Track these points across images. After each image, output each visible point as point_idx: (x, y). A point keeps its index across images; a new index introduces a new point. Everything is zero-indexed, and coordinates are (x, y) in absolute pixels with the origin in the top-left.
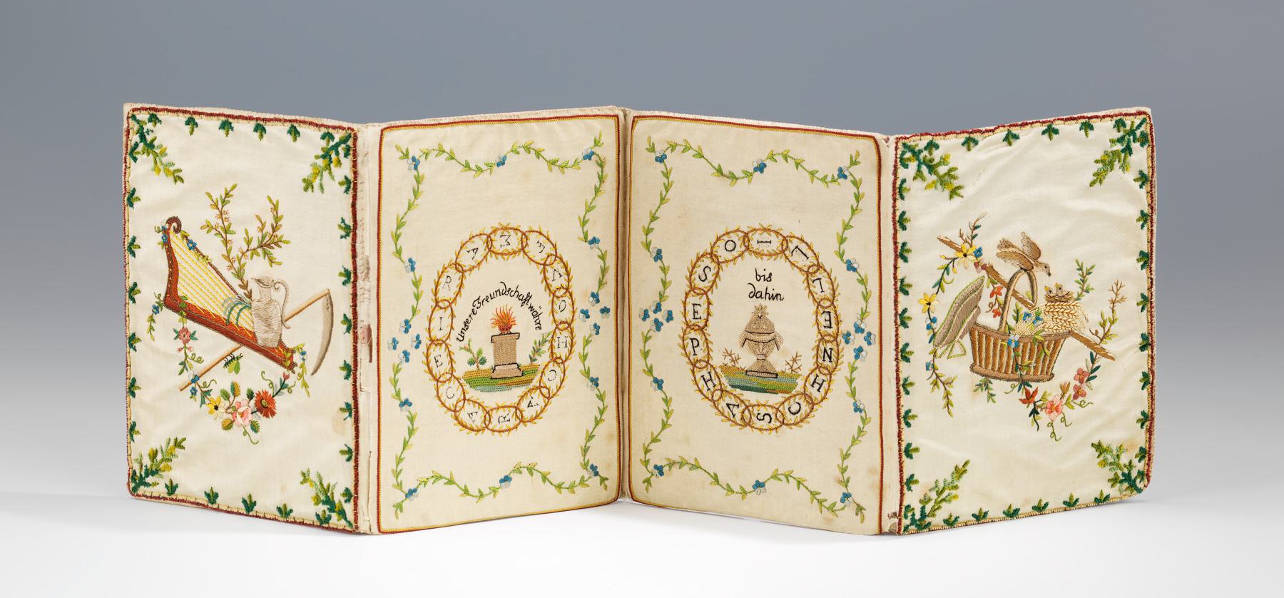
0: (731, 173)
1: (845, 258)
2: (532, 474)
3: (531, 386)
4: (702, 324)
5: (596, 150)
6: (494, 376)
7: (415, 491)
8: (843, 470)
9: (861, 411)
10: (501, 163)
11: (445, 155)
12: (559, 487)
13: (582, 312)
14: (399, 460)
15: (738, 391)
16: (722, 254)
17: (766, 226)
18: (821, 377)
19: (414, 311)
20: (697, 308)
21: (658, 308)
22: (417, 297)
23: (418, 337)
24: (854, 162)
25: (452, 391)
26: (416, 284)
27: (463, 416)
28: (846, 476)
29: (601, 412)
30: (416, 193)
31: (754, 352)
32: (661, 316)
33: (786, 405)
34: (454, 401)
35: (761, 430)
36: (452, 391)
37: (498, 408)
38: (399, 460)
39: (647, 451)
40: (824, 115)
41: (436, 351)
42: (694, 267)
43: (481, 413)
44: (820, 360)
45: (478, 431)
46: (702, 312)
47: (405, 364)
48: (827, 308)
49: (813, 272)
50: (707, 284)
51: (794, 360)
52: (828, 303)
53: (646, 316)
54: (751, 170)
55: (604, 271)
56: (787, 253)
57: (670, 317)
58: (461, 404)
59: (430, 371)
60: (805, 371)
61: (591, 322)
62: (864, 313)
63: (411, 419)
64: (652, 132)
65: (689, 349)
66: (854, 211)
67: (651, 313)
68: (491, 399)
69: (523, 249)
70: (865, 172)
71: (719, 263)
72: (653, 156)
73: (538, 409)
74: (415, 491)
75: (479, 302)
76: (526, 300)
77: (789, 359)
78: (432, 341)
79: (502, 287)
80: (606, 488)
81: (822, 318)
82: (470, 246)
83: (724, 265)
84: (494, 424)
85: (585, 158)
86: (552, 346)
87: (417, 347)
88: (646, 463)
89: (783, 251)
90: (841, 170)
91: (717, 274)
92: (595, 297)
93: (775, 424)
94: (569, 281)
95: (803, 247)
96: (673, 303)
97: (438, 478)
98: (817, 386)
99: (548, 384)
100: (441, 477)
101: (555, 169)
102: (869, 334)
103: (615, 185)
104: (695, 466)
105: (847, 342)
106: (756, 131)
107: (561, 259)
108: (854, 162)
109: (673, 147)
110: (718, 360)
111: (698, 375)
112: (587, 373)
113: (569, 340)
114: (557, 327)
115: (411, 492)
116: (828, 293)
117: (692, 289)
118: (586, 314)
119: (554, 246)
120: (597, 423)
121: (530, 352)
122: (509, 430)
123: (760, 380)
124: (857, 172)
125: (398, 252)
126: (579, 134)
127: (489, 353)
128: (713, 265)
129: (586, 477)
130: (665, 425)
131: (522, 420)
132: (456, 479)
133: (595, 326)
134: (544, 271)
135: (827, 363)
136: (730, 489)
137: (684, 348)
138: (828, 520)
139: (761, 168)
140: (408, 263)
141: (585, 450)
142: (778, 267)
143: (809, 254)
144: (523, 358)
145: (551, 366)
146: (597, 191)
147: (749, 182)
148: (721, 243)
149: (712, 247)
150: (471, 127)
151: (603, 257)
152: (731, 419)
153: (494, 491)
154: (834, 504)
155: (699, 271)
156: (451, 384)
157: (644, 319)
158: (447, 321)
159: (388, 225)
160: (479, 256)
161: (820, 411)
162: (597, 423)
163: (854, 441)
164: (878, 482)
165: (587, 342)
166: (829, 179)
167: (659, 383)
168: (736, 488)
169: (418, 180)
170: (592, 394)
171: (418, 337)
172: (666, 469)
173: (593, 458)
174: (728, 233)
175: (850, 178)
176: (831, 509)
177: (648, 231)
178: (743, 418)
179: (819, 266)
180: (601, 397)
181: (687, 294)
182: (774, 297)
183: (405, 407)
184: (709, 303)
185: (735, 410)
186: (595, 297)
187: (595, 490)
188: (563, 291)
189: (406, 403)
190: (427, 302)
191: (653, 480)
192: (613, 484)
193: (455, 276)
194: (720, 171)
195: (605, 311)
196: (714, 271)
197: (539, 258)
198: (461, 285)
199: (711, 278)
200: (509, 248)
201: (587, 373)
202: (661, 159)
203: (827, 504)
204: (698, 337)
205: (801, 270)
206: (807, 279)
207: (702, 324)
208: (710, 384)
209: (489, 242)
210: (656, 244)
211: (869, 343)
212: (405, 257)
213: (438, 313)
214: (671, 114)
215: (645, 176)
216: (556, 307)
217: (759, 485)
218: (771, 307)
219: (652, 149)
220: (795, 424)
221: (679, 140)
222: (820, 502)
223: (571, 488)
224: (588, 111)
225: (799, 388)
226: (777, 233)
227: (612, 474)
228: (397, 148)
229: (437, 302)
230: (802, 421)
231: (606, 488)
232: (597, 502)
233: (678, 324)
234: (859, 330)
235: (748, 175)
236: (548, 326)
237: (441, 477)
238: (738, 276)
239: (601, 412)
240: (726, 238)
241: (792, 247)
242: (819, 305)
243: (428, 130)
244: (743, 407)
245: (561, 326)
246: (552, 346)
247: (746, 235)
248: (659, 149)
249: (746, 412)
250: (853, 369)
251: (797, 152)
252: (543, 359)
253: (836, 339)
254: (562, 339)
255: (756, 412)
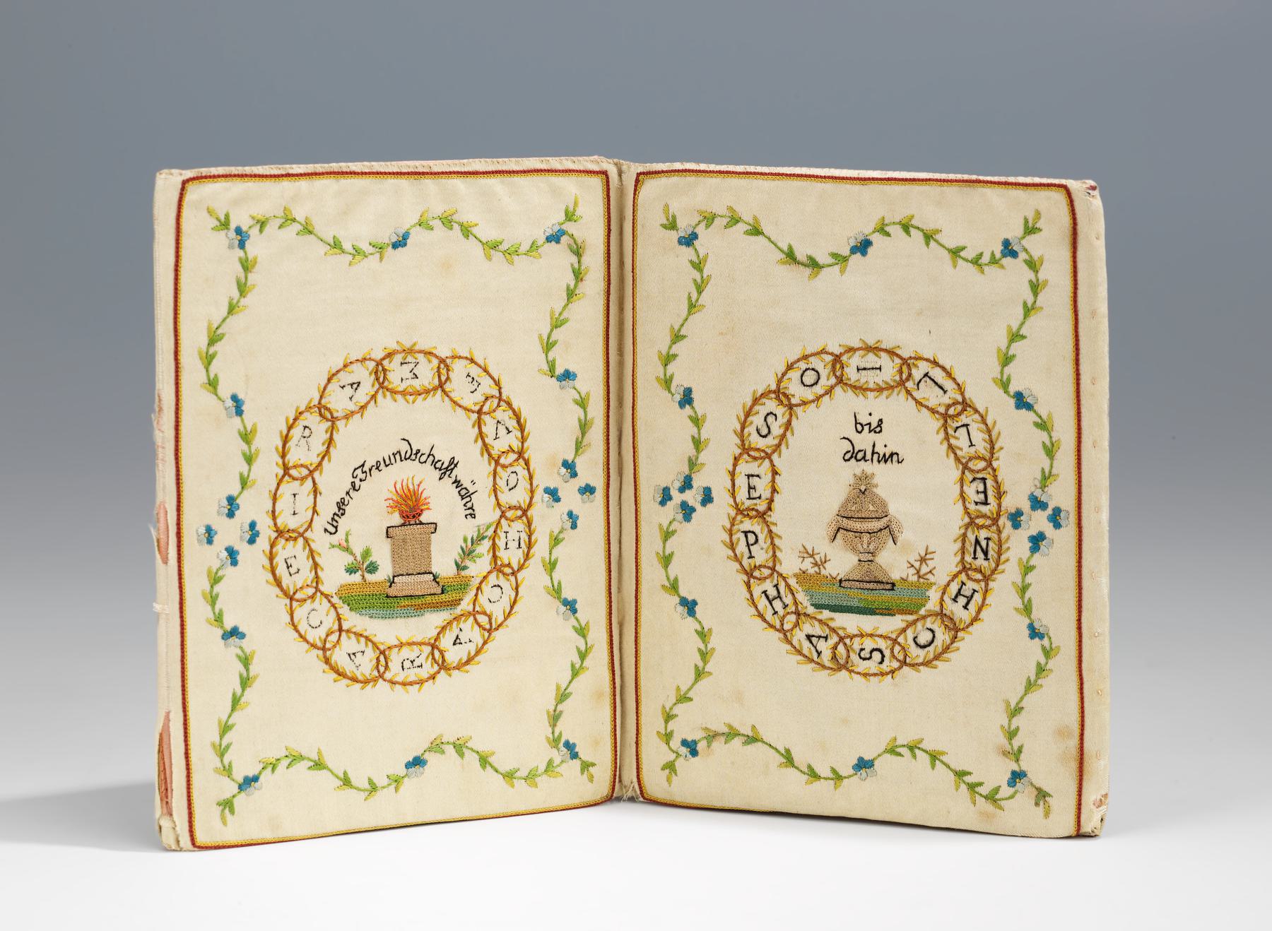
0: (810, 258)
1: (1013, 389)
2: (461, 755)
3: (458, 610)
4: (762, 506)
5: (569, 227)
6: (392, 592)
7: (255, 779)
8: (1011, 734)
9: (1041, 636)
10: (400, 243)
11: (297, 227)
12: (509, 776)
13: (548, 491)
14: (225, 729)
15: (826, 614)
16: (796, 390)
17: (871, 342)
18: (970, 585)
19: (244, 483)
20: (754, 481)
21: (687, 484)
22: (249, 460)
23: (253, 525)
24: (1030, 230)
25: (317, 618)
26: (246, 437)
27: (339, 657)
28: (1016, 743)
29: (583, 656)
30: (242, 288)
31: (854, 550)
32: (692, 497)
33: (910, 634)
34: (322, 632)
35: (865, 675)
36: (317, 618)
37: (401, 645)
38: (225, 729)
39: (669, 717)
40: (971, 155)
41: (285, 550)
42: (748, 415)
43: (371, 654)
44: (968, 558)
45: (366, 682)
46: (762, 487)
47: (229, 571)
48: (980, 472)
49: (955, 413)
50: (771, 441)
51: (923, 560)
52: (982, 464)
53: (666, 497)
54: (846, 252)
55: (584, 426)
56: (910, 385)
57: (707, 498)
58: (334, 638)
59: (278, 583)
60: (941, 578)
61: (562, 508)
62: (1046, 478)
63: (246, 661)
64: (669, 196)
65: (741, 548)
66: (1028, 310)
67: (674, 493)
68: (387, 630)
69: (441, 385)
70: (1049, 246)
71: (791, 407)
72: (674, 235)
73: (472, 648)
74: (255, 779)
75: (363, 471)
76: (447, 469)
77: (913, 558)
78: (280, 533)
79: (404, 447)
80: (591, 778)
81: (972, 491)
82: (345, 378)
83: (799, 410)
84: (394, 671)
85: (549, 239)
86: (494, 546)
87: (252, 541)
88: (668, 737)
89: (902, 383)
90: (1006, 243)
91: (789, 423)
92: (569, 466)
93: (889, 664)
94: (523, 440)
95: (938, 374)
96: (713, 475)
97: (295, 759)
98: (962, 601)
99: (489, 608)
100: (301, 758)
101: (497, 256)
102: (1057, 511)
103: (601, 285)
104: (752, 739)
105: (1016, 525)
106: (856, 188)
107: (509, 404)
108: (1030, 230)
109: (709, 219)
110: (790, 564)
111: (757, 591)
112: (556, 591)
113: (524, 537)
114: (503, 515)
115: (249, 782)
116: (981, 447)
117: (746, 449)
118: (553, 494)
119: (497, 383)
120: (575, 673)
121: (455, 554)
122: (421, 682)
123: (865, 595)
124: (1034, 245)
125: (213, 384)
126: (538, 200)
127: (383, 556)
128: (780, 411)
129: (557, 760)
130: (699, 674)
131: (443, 666)
132: (329, 761)
133: (570, 514)
134: (479, 423)
135: (980, 561)
136: (813, 775)
137: (732, 547)
138: (986, 816)
139: (863, 247)
140: (230, 403)
141: (555, 718)
142: (894, 409)
143: (948, 385)
144: (443, 564)
145: (493, 579)
146: (571, 294)
147: (842, 272)
148: (794, 375)
149: (779, 382)
150: (346, 182)
151: (582, 403)
152: (813, 660)
153: (397, 781)
154: (997, 790)
155: (757, 420)
156: (316, 604)
157: (663, 503)
158: (305, 500)
159: (194, 339)
160: (362, 396)
161: (967, 642)
162: (575, 673)
163: (1030, 686)
164: (1074, 752)
165: (556, 541)
166: (986, 259)
167: (690, 606)
168: (824, 771)
169: (247, 266)
170: (564, 628)
171: (253, 525)
172: (701, 747)
173: (567, 729)
174: (805, 357)
175: (1023, 256)
176: (992, 798)
177: (668, 359)
178: (834, 658)
179: (966, 405)
180: (582, 631)
181: (736, 459)
182: (885, 459)
183: (234, 640)
184: (775, 473)
185: (822, 645)
186: (569, 466)
187: (570, 782)
188: (512, 457)
189: (235, 633)
190: (267, 468)
191: (680, 764)
192: (603, 773)
193: (320, 429)
194: (790, 256)
195: (588, 490)
196: (782, 420)
197: (470, 401)
198: (330, 442)
199: (777, 430)
200: (417, 384)
201: (556, 591)
202: (689, 240)
203: (984, 790)
204: (757, 529)
205: (933, 411)
206: (945, 426)
207: (762, 506)
208: (778, 605)
209: (380, 372)
210: (682, 379)
211: (1057, 525)
212: (225, 391)
213: (288, 488)
214: (703, 167)
215: (661, 270)
216: (501, 483)
217: (863, 765)
218: (883, 475)
219: (672, 225)
220: (927, 663)
221: (720, 209)
222: (972, 787)
223: (531, 778)
224: (555, 163)
225: (933, 605)
226: (892, 353)
227: (603, 759)
228: (210, 212)
229: (286, 469)
230: (937, 658)
231: (591, 778)
232: (577, 801)
233: (722, 508)
234: (1037, 504)
235: (840, 260)
236: (487, 513)
237: (301, 758)
238: (824, 426)
239: (583, 656)
240: (803, 365)
241: (917, 374)
242: (965, 467)
243: (268, 184)
244: (835, 639)
245: (509, 514)
246: (494, 546)
247: (837, 359)
248: (684, 224)
249: (841, 648)
250: (1028, 569)
251: (928, 216)
252: (479, 567)
253: (995, 521)
254: (513, 535)
255: (857, 647)
